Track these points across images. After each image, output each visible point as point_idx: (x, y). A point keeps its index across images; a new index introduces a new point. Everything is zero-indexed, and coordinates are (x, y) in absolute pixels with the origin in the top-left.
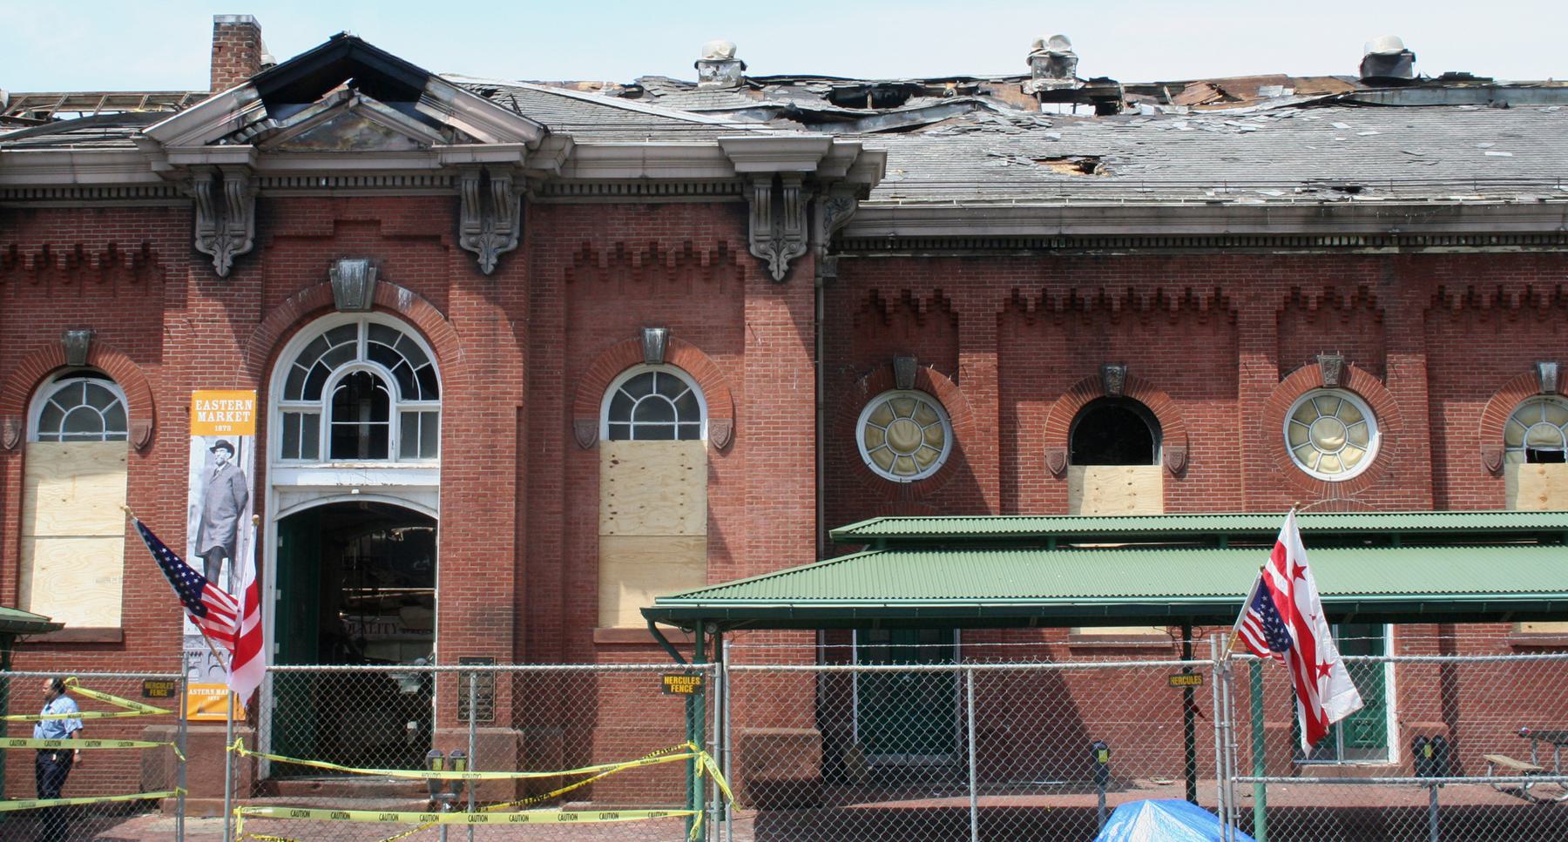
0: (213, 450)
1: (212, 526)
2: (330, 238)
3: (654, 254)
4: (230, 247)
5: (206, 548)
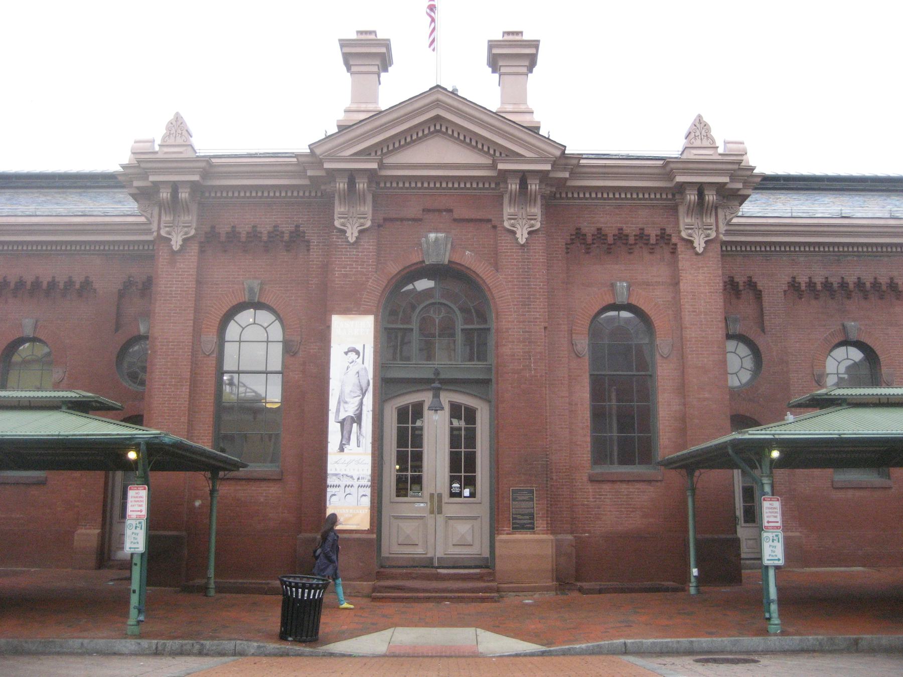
0: (346, 353)
1: (346, 403)
2: (420, 220)
3: (621, 236)
4: (357, 225)
5: (342, 416)
